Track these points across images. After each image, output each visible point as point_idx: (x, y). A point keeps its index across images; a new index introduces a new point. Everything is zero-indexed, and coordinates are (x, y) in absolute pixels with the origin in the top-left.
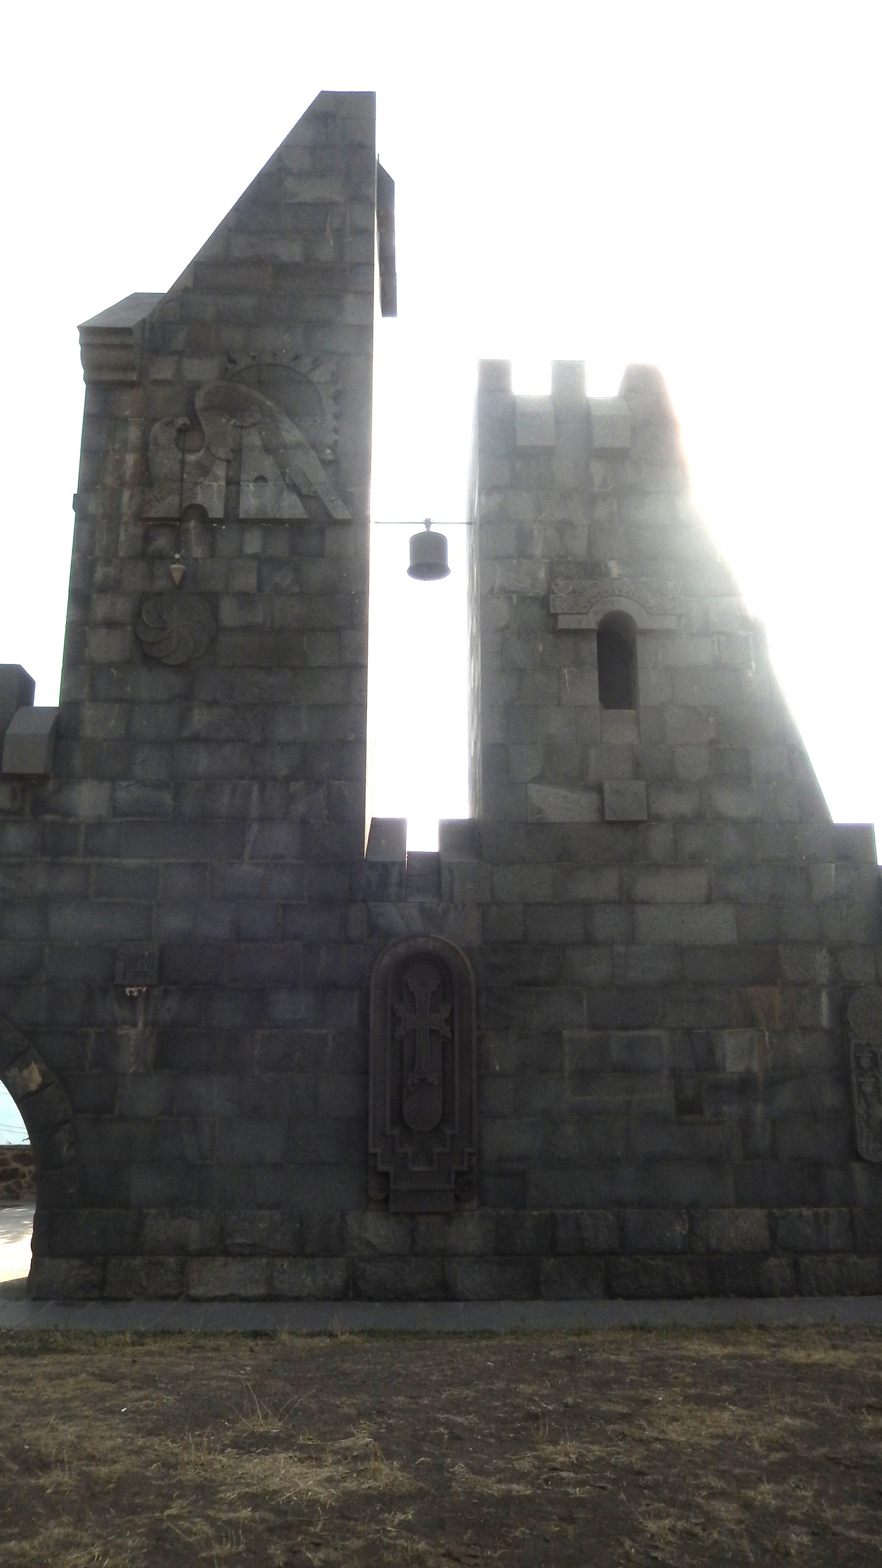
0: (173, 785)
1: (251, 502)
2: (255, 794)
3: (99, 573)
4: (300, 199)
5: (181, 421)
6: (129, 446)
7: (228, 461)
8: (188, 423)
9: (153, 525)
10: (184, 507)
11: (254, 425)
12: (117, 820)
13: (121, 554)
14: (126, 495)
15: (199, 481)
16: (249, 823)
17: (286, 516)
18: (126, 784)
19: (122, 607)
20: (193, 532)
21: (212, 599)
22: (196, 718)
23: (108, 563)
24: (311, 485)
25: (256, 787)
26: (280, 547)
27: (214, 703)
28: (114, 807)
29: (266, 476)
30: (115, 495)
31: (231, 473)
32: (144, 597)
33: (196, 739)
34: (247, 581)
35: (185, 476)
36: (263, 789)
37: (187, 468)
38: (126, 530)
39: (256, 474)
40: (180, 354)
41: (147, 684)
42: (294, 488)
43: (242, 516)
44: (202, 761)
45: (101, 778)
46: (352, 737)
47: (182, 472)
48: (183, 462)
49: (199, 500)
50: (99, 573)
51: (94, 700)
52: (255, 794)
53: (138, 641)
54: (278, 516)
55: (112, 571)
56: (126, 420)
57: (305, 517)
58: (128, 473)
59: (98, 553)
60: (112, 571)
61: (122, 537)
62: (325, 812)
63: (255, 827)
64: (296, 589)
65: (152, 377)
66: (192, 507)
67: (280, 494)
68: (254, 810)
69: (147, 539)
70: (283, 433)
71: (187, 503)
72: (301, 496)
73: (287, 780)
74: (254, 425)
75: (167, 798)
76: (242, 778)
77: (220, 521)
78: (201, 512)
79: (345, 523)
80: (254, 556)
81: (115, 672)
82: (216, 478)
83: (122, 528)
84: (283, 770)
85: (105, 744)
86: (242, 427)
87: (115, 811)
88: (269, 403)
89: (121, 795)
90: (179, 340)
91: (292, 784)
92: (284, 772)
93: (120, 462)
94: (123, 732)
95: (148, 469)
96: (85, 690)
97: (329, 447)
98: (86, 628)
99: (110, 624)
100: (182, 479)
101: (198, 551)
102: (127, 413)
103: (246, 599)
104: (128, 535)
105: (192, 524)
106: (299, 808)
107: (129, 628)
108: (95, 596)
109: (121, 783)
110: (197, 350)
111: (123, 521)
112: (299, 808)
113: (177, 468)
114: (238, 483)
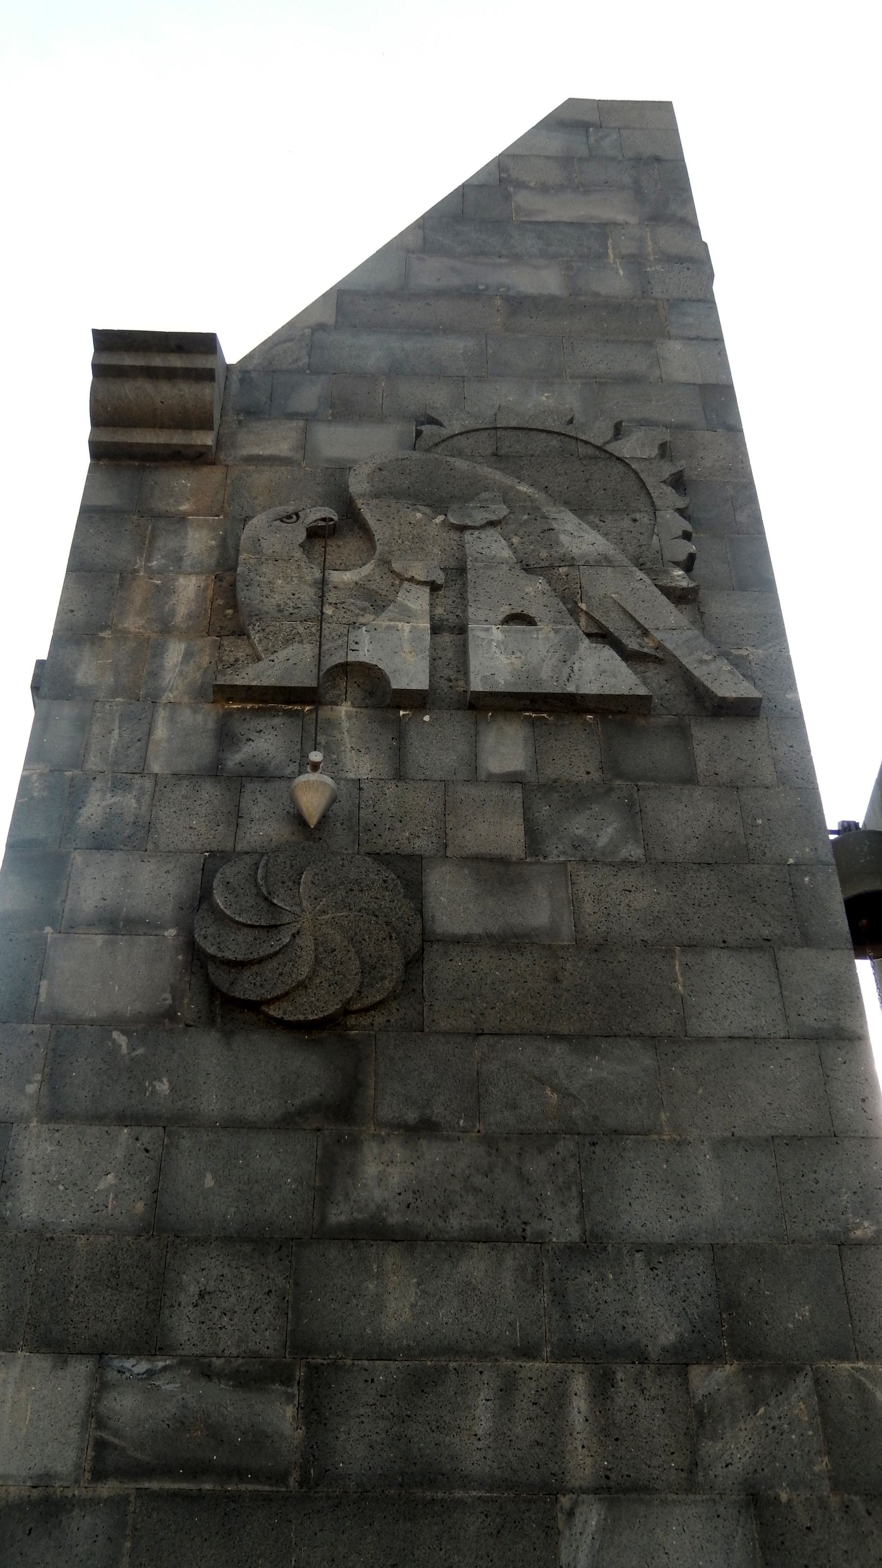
0: (300, 1373)
1: (496, 660)
2: (579, 1405)
3: (95, 808)
4: (550, 218)
5: (315, 514)
6: (187, 562)
7: (434, 587)
8: (336, 518)
9: (243, 710)
10: (324, 669)
11: (492, 524)
12: (108, 1489)
13: (156, 767)
14: (175, 652)
15: (361, 620)
16: (565, 1501)
17: (591, 688)
18: (143, 1366)
19: (155, 885)
20: (345, 725)
21: (407, 872)
22: (371, 1170)
23: (118, 784)
24: (645, 633)
25: (579, 1384)
26: (576, 756)
27: (425, 1128)
28: (101, 1445)
29: (532, 612)
30: (150, 650)
31: (440, 610)
32: (213, 861)
33: (373, 1232)
34: (500, 830)
35: (329, 611)
36: (602, 1387)
37: (332, 597)
38: (171, 719)
39: (506, 610)
40: (309, 418)
41: (224, 1075)
42: (602, 636)
43: (477, 685)
44: (397, 1301)
45: (56, 1346)
46: (728, 685)
47: (322, 599)
48: (322, 584)
49: (366, 651)
50: (95, 808)
51: (55, 1115)
52: (579, 1405)
53: (196, 957)
54: (571, 689)
55: (129, 803)
56: (182, 519)
57: (642, 691)
58: (182, 610)
59: (93, 763)
60: (129, 803)
61: (161, 732)
62: (822, 1465)
63: (591, 1516)
64: (634, 851)
65: (245, 452)
66: (345, 669)
67: (571, 646)
68: (582, 1461)
69: (225, 737)
70: (563, 538)
71: (337, 659)
72: (628, 656)
73: (680, 1360)
74: (492, 524)
75: (282, 1416)
76: (528, 1352)
77: (418, 701)
78: (368, 682)
79: (744, 710)
80: (512, 780)
81: (121, 1040)
82: (407, 615)
83: (162, 714)
84: (661, 1324)
85: (81, 1241)
86: (462, 529)
87: (104, 1457)
88: (523, 488)
89: (124, 1405)
90: (308, 397)
91: (696, 1372)
92: (668, 1337)
93: (165, 591)
94: (140, 1206)
95: (233, 602)
96: (31, 1089)
97: (677, 564)
98: (48, 929)
99: (117, 924)
100: (321, 618)
101: (360, 765)
102: (184, 508)
103: (496, 871)
104: (177, 731)
105: (344, 709)
106: (735, 1450)
107: (171, 932)
108: (78, 858)
109: (128, 1364)
110: (343, 410)
111: (164, 699)
112: (735, 1450)
113: (308, 594)
114: (462, 630)
